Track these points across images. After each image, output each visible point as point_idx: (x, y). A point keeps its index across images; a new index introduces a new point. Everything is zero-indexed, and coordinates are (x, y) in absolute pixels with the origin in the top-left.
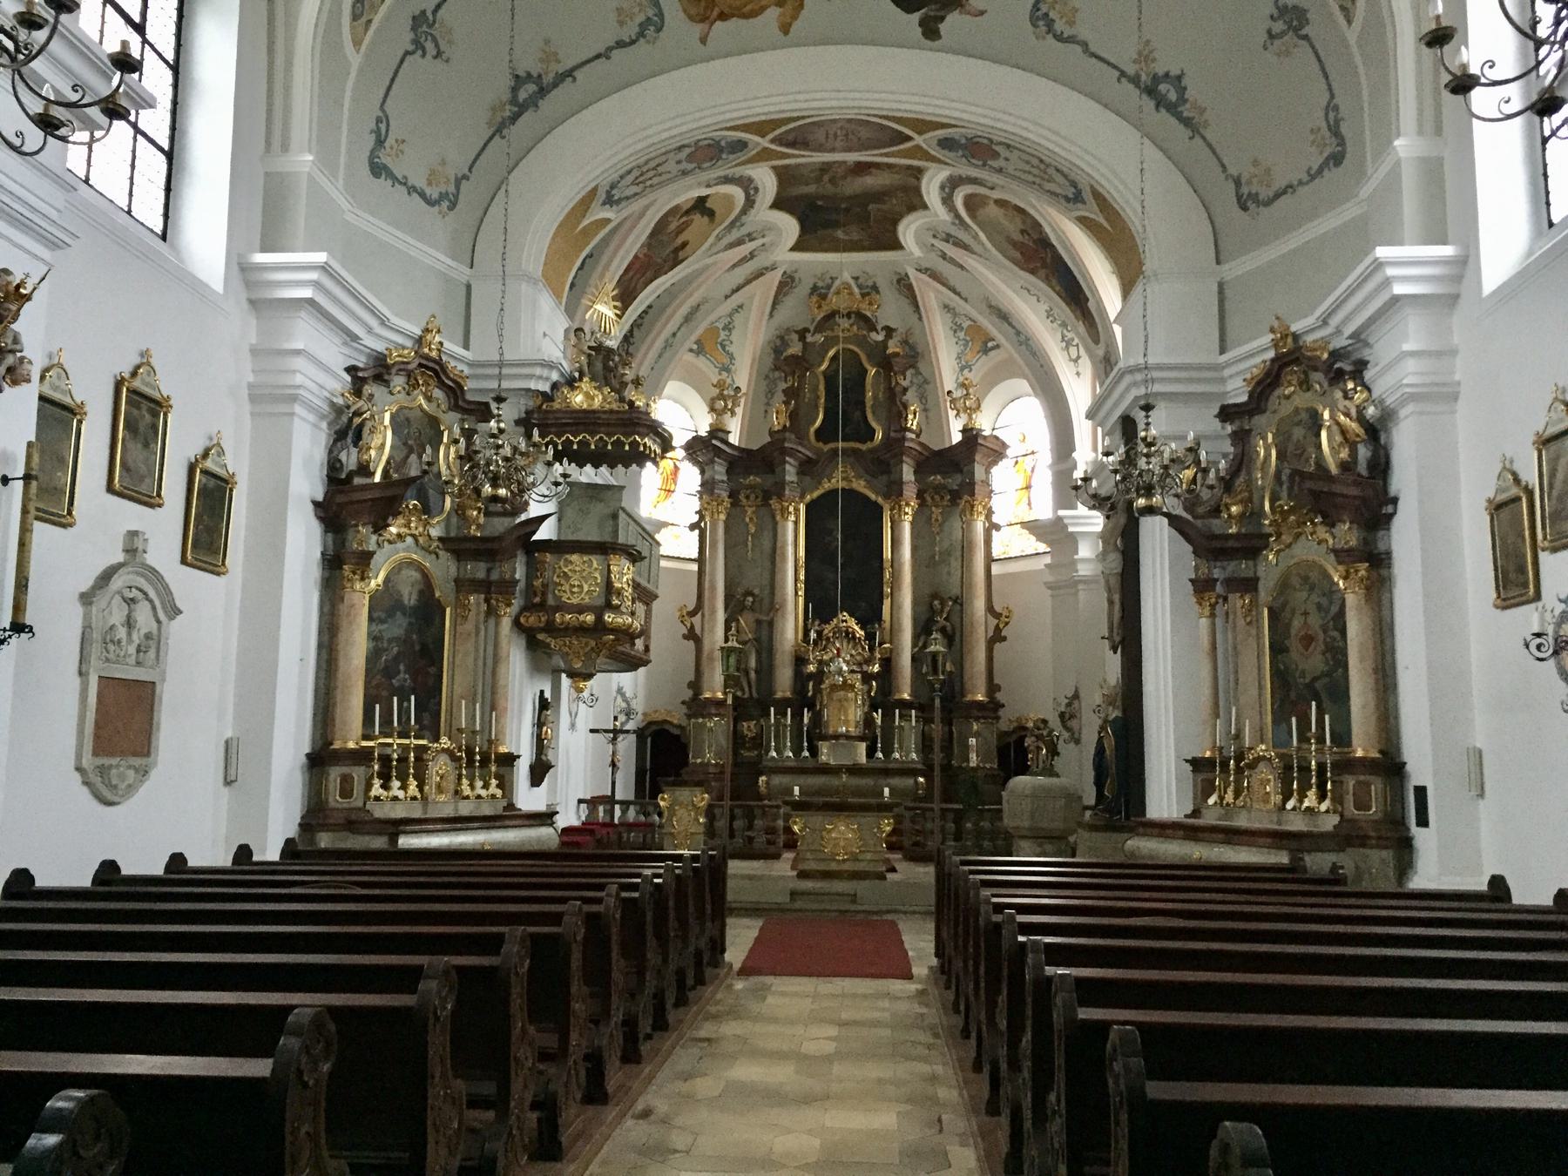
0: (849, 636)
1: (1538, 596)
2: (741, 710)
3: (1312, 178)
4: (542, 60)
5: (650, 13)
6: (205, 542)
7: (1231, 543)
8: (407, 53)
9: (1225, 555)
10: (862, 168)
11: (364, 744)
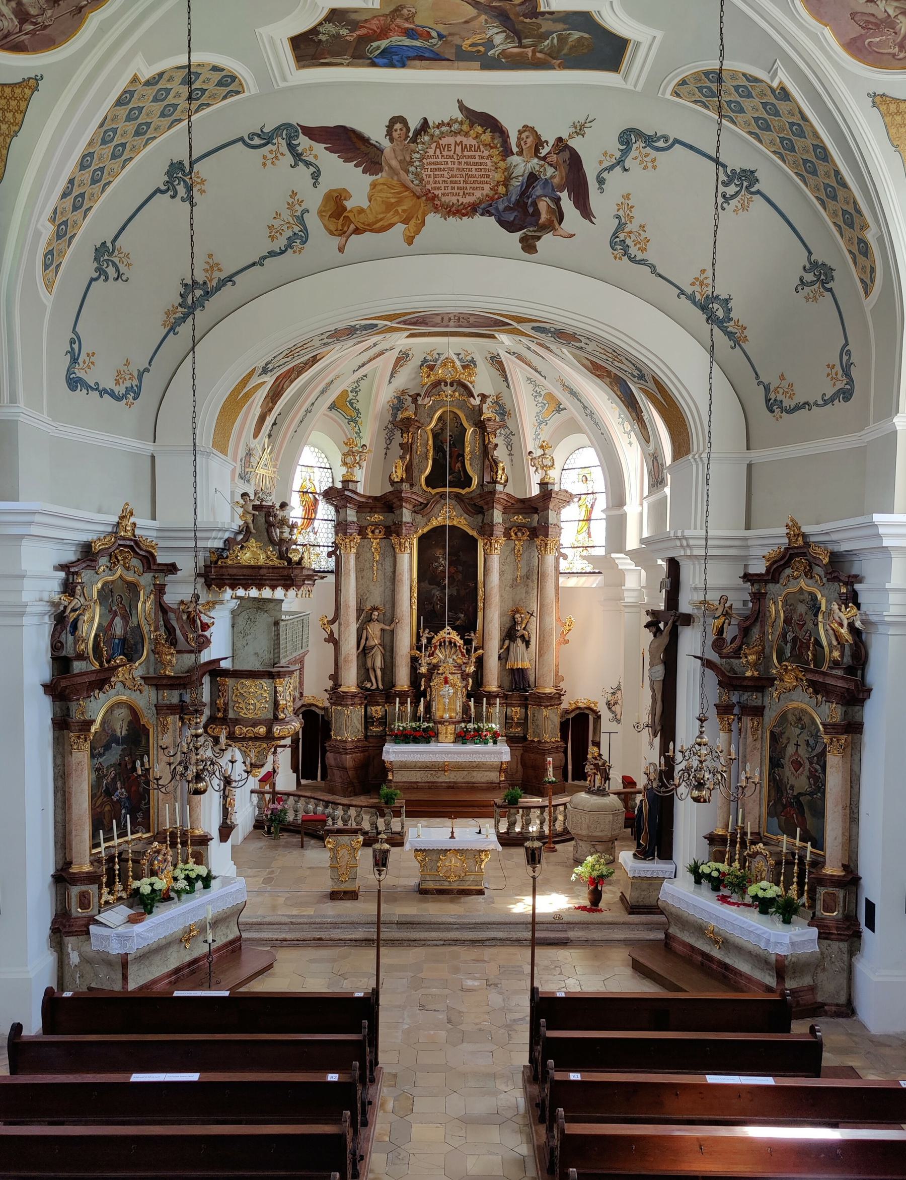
2: (368, 697)
3: (826, 403)
4: (206, 271)
9: (740, 692)
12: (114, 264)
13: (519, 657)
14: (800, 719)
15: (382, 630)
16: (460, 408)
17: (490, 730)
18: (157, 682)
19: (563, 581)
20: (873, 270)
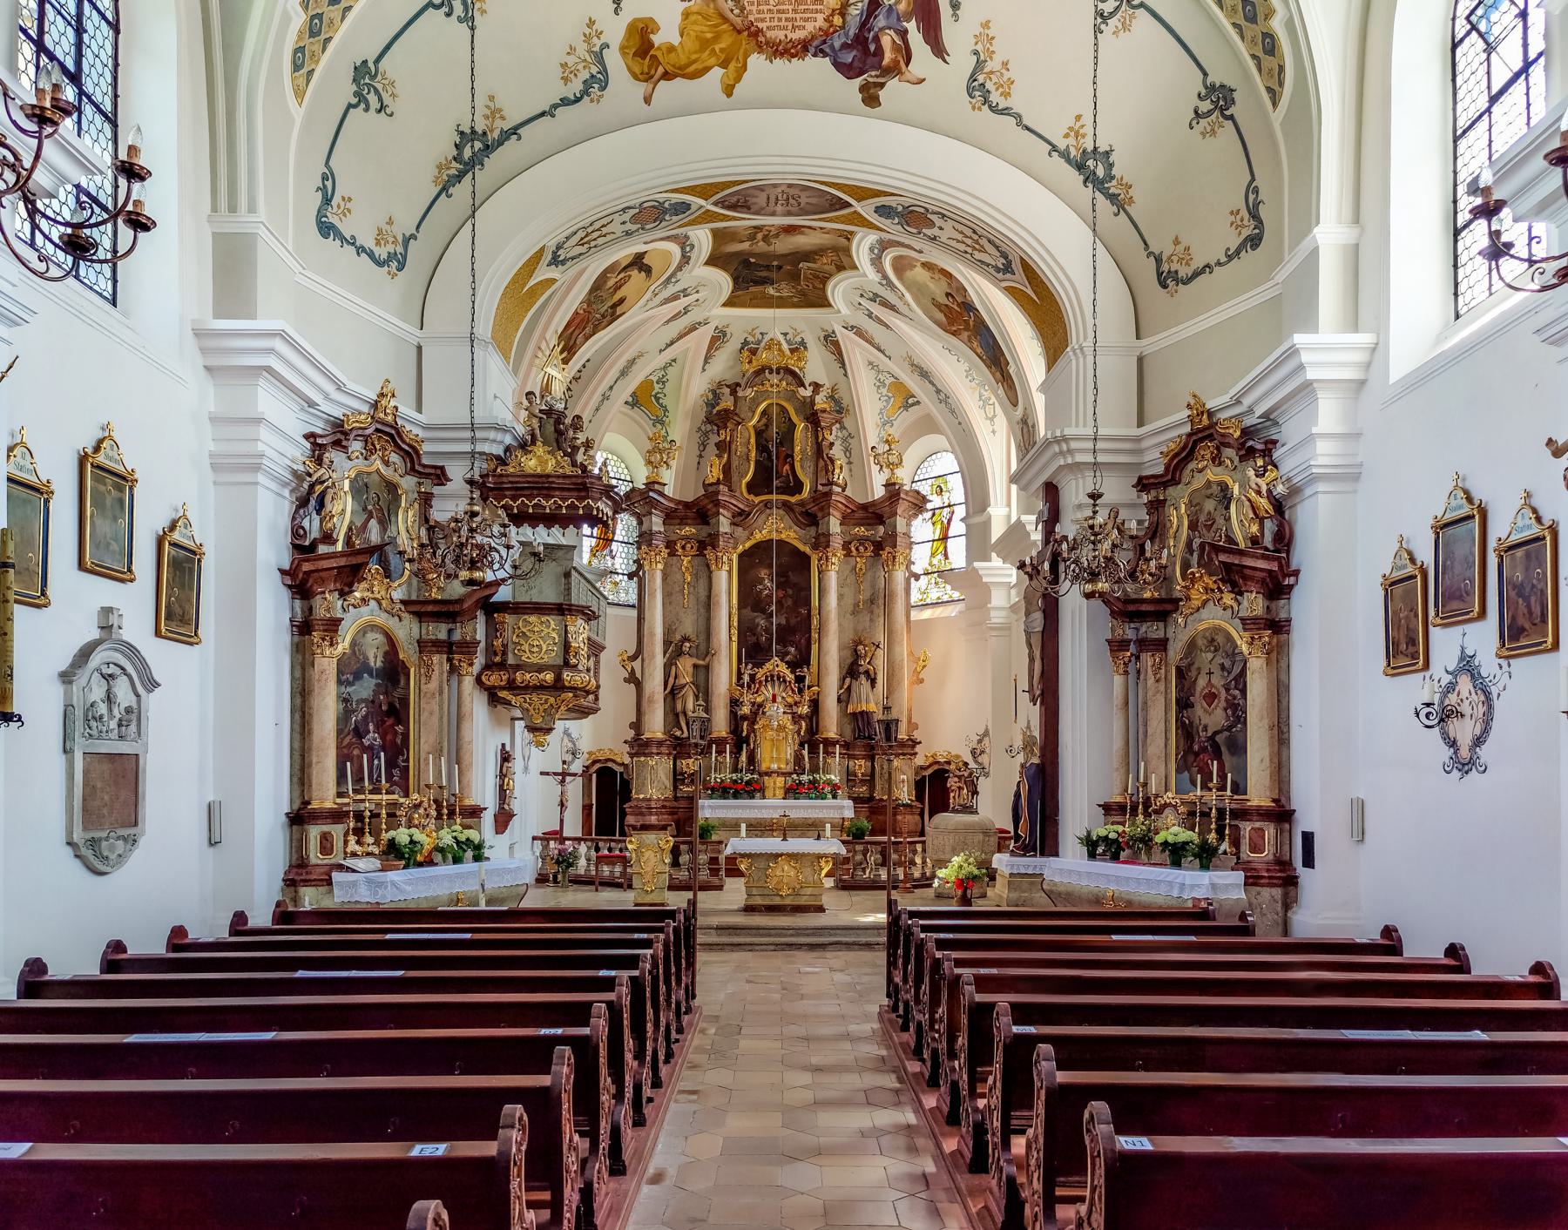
0: (782, 679)
1: (1427, 666)
3: (1230, 258)
4: (486, 117)
5: (594, 70)
6: (177, 616)
7: (1144, 607)
8: (350, 106)
9: (1139, 619)
10: (790, 230)
11: (339, 801)
12: (377, 91)
13: (864, 697)
14: (1213, 640)
15: (695, 666)
16: (788, 400)
17: (829, 783)
18: (420, 609)
19: (915, 615)
20: (1281, 68)
